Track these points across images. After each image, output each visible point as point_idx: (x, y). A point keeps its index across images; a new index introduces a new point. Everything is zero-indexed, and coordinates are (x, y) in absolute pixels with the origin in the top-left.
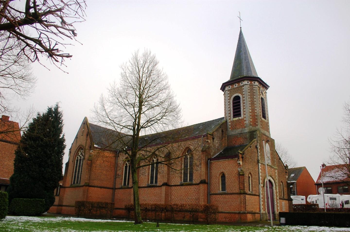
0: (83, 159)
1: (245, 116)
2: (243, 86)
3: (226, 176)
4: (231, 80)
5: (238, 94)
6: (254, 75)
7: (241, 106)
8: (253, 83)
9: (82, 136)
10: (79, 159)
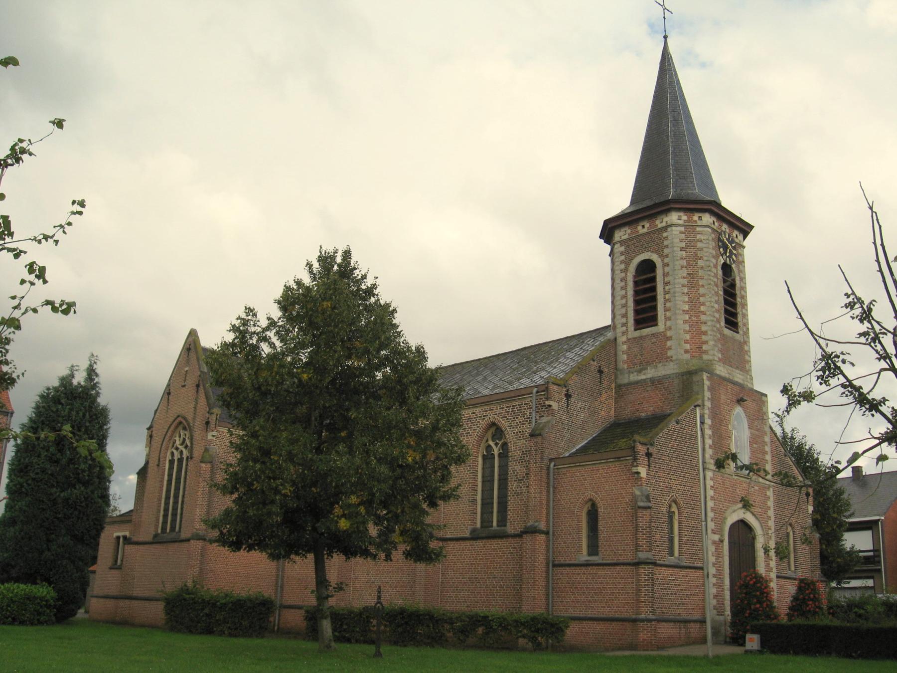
0: (187, 457)
1: (669, 323)
2: (665, 229)
3: (601, 510)
4: (629, 211)
5: (649, 253)
6: (697, 192)
7: (658, 292)
8: (696, 218)
9: (184, 389)
10: (176, 458)
